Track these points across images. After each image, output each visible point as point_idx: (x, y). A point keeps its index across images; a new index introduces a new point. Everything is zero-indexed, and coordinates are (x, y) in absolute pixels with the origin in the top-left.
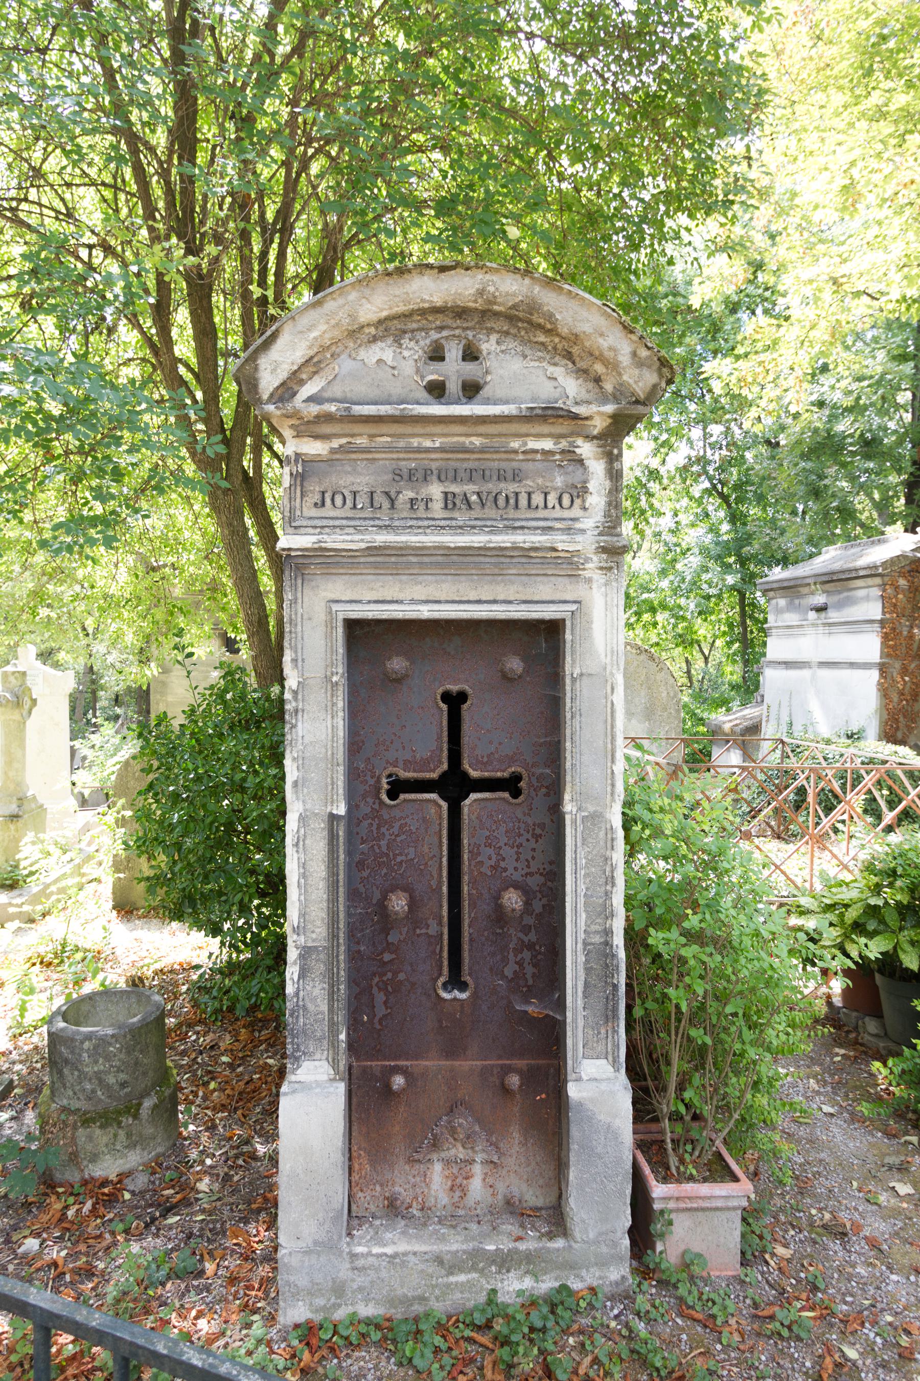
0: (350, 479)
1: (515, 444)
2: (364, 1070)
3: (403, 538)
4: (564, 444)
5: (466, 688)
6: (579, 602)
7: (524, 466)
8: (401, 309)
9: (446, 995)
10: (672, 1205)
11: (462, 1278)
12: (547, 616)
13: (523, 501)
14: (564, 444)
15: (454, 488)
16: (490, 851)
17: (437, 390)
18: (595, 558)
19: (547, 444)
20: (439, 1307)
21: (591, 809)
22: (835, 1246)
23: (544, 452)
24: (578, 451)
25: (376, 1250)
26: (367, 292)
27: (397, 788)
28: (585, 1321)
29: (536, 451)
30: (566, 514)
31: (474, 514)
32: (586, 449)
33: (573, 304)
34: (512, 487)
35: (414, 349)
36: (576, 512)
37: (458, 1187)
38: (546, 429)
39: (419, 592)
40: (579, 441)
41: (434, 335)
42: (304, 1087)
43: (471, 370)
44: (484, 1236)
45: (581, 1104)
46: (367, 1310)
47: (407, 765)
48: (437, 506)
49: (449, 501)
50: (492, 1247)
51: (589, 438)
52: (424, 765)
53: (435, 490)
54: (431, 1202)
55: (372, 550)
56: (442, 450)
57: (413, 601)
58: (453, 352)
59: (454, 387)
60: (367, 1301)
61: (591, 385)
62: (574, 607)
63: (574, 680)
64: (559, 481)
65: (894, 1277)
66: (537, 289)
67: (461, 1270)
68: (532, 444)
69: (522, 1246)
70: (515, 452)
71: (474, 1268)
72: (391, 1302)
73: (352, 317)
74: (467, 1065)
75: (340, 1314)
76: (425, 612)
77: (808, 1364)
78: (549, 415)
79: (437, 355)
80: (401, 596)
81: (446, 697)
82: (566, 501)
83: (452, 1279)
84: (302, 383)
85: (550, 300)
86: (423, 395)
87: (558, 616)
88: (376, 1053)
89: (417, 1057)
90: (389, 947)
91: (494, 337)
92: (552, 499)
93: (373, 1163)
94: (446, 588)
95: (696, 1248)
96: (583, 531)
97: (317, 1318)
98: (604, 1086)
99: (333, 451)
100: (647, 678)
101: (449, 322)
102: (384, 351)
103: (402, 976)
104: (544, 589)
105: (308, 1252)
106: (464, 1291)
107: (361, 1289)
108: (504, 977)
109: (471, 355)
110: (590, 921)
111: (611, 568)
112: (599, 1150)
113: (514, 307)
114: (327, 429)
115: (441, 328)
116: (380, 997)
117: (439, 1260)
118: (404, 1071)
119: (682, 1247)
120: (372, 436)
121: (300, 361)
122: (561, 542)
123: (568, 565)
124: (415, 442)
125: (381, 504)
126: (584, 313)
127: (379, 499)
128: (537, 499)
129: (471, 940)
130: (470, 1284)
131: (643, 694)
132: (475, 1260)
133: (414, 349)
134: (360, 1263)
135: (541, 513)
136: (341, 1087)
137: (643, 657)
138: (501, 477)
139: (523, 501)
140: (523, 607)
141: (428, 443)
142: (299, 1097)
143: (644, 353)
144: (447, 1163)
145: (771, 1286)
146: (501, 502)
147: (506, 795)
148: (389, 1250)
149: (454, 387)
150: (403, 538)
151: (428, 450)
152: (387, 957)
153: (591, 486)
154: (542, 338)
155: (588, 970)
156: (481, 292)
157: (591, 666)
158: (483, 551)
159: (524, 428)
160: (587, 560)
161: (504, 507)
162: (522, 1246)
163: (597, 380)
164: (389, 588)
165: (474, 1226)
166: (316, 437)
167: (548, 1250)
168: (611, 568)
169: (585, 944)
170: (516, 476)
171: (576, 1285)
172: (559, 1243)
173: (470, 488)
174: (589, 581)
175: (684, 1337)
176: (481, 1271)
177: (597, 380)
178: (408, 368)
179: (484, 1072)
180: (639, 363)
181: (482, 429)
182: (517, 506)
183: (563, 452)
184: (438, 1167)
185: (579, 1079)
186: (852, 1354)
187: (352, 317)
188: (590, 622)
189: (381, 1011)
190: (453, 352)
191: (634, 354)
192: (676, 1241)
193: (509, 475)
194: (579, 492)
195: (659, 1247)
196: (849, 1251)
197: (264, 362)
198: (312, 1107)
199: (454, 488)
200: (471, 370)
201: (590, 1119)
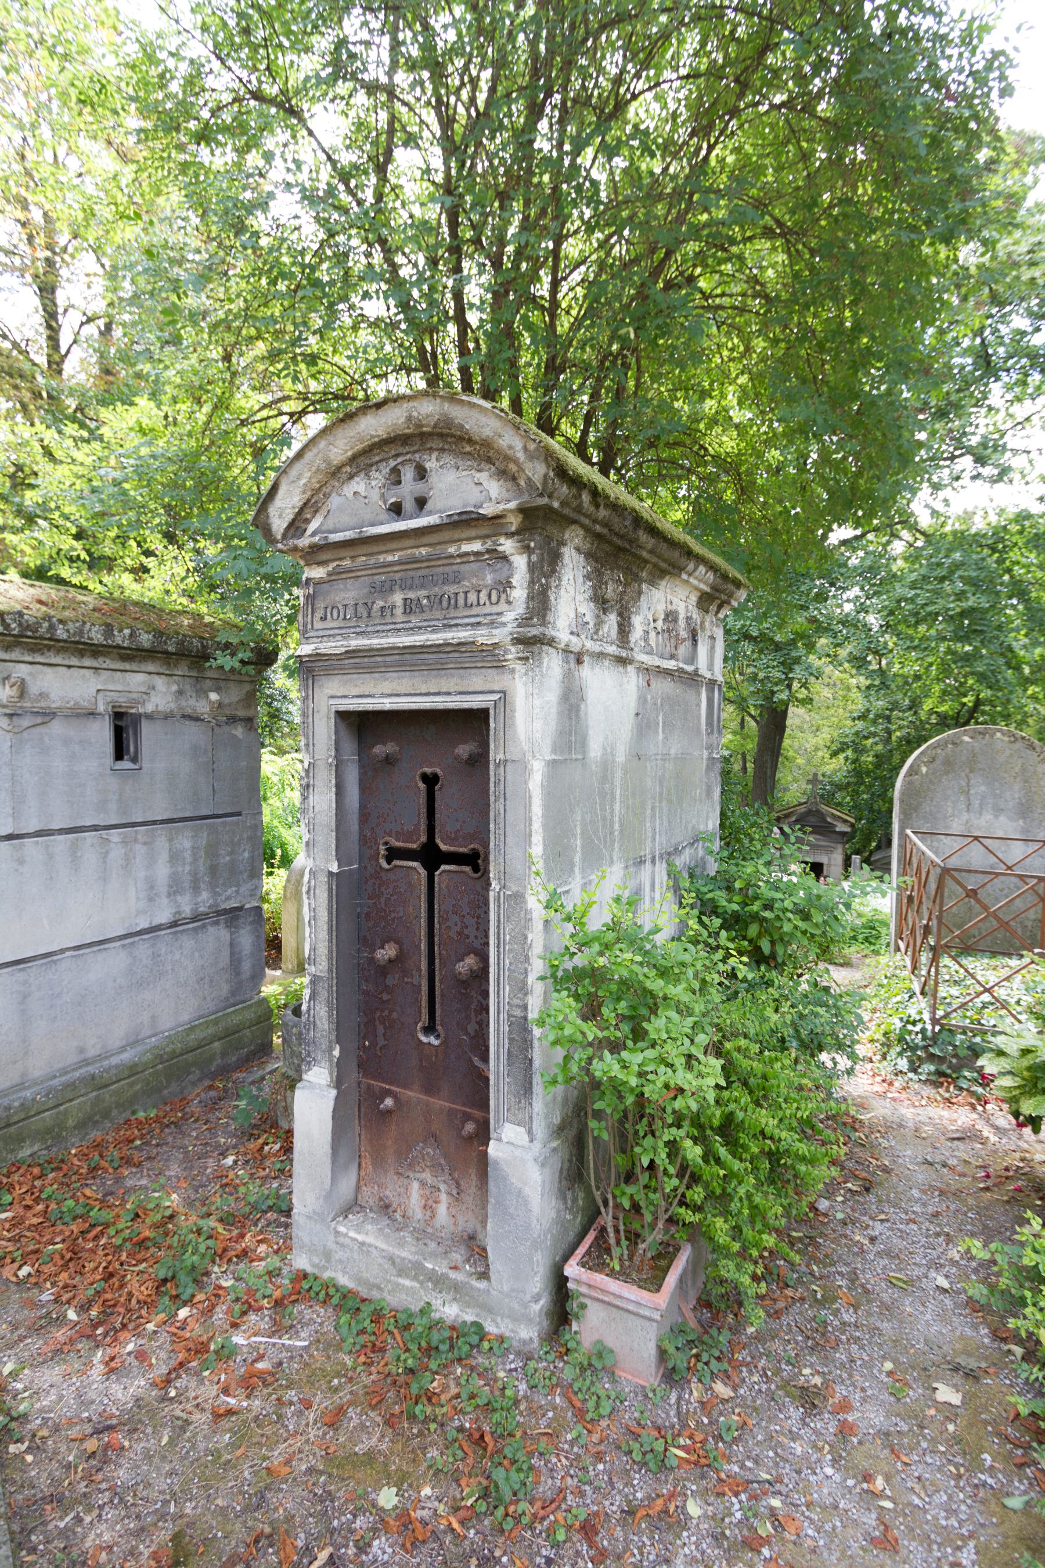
0: (343, 595)
1: (452, 550)
2: (369, 1087)
3: (392, 640)
4: (489, 544)
5: (438, 770)
6: (504, 692)
7: (463, 568)
8: (359, 447)
9: (424, 1039)
10: (584, 1289)
11: (407, 1283)
12: (475, 705)
13: (461, 602)
14: (489, 544)
15: (411, 595)
16: (456, 918)
17: (397, 510)
18: (513, 649)
19: (476, 546)
20: (393, 1300)
21: (515, 889)
22: (795, 1413)
23: (477, 554)
24: (500, 549)
25: (352, 1234)
26: (331, 438)
27: (393, 854)
28: (481, 1360)
29: (467, 554)
30: (495, 609)
31: (425, 616)
32: (507, 545)
33: (475, 414)
34: (452, 589)
35: (379, 477)
36: (503, 606)
37: (429, 1207)
38: (473, 533)
39: (387, 687)
40: (502, 540)
41: (392, 463)
42: (312, 1086)
43: (420, 488)
44: (433, 1255)
45: (496, 1163)
46: (344, 1281)
47: (398, 836)
48: (399, 611)
49: (409, 607)
50: (429, 1266)
51: (510, 535)
52: (409, 837)
53: (398, 598)
54: (410, 1213)
55: (351, 653)
56: (399, 563)
57: (384, 695)
58: (408, 474)
59: (409, 505)
60: (345, 1273)
61: (510, 484)
62: (496, 697)
63: (498, 765)
64: (489, 579)
65: (829, 1471)
66: (446, 405)
67: (407, 1276)
68: (466, 548)
69: (453, 1275)
70: (451, 557)
71: (415, 1278)
72: (359, 1281)
73: (326, 460)
74: (440, 1103)
75: (326, 1275)
76: (387, 704)
77: (639, 1495)
78: (467, 522)
79: (395, 478)
80: (374, 691)
81: (425, 777)
82: (494, 598)
83: (401, 1281)
84: (308, 521)
85: (458, 414)
86: (384, 516)
87: (483, 705)
88: (379, 1076)
89: (405, 1086)
90: (387, 989)
91: (434, 455)
92: (483, 596)
93: (374, 1165)
94: (403, 682)
95: (610, 1342)
96: (504, 624)
97: (309, 1269)
98: (518, 1152)
99: (329, 574)
100: (1024, 769)
101: (401, 450)
102: (358, 485)
103: (395, 1015)
104: (477, 680)
105: (309, 1218)
106: (404, 1294)
107: (340, 1261)
108: (467, 1033)
109: (422, 473)
110: (513, 995)
111: (527, 659)
112: (512, 1210)
113: (435, 426)
114: (324, 556)
115: (397, 456)
116: (380, 1029)
117: (391, 1259)
118: (395, 1096)
119: (596, 1337)
120: (353, 558)
121: (300, 504)
122: (482, 636)
123: (488, 657)
124: (381, 558)
125: (363, 615)
126: (484, 420)
127: (361, 609)
128: (472, 597)
129: (442, 995)
130: (409, 1291)
131: (1016, 787)
132: (415, 1270)
133: (379, 477)
134: (341, 1240)
135: (475, 611)
136: (334, 1092)
137: (1019, 745)
138: (446, 581)
139: (461, 602)
140: (458, 698)
141: (390, 558)
142: (306, 1092)
143: (532, 446)
144: (423, 1184)
145: (679, 1414)
146: (445, 604)
147: (467, 869)
148: (360, 1238)
149: (409, 505)
150: (392, 640)
151: (391, 564)
152: (385, 997)
153: (514, 582)
154: (468, 449)
155: (511, 1040)
156: (409, 418)
157: (513, 753)
158: (424, 649)
159: (457, 534)
160: (506, 651)
161: (446, 608)
162: (453, 1275)
163: (514, 479)
164: (367, 684)
165: (433, 1245)
166: (320, 563)
167: (472, 1288)
168: (527, 659)
169: (509, 1016)
170: (457, 580)
171: (490, 1328)
172: (482, 1285)
173: (424, 593)
174: (513, 671)
175: (550, 1414)
176: (421, 1283)
177: (514, 479)
178: (375, 495)
179: (451, 1112)
180: (531, 457)
181: (426, 540)
182: (456, 606)
183: (488, 551)
184: (416, 1185)
185: (499, 1140)
186: (694, 1509)
187: (326, 460)
188: (513, 711)
189: (381, 1042)
190: (408, 474)
191: (525, 448)
192: (592, 1326)
193: (451, 578)
194: (505, 585)
195: (575, 1327)
196: (805, 1424)
197: (273, 510)
198: (314, 1105)
199: (411, 595)
200: (420, 488)
201: (505, 1178)
